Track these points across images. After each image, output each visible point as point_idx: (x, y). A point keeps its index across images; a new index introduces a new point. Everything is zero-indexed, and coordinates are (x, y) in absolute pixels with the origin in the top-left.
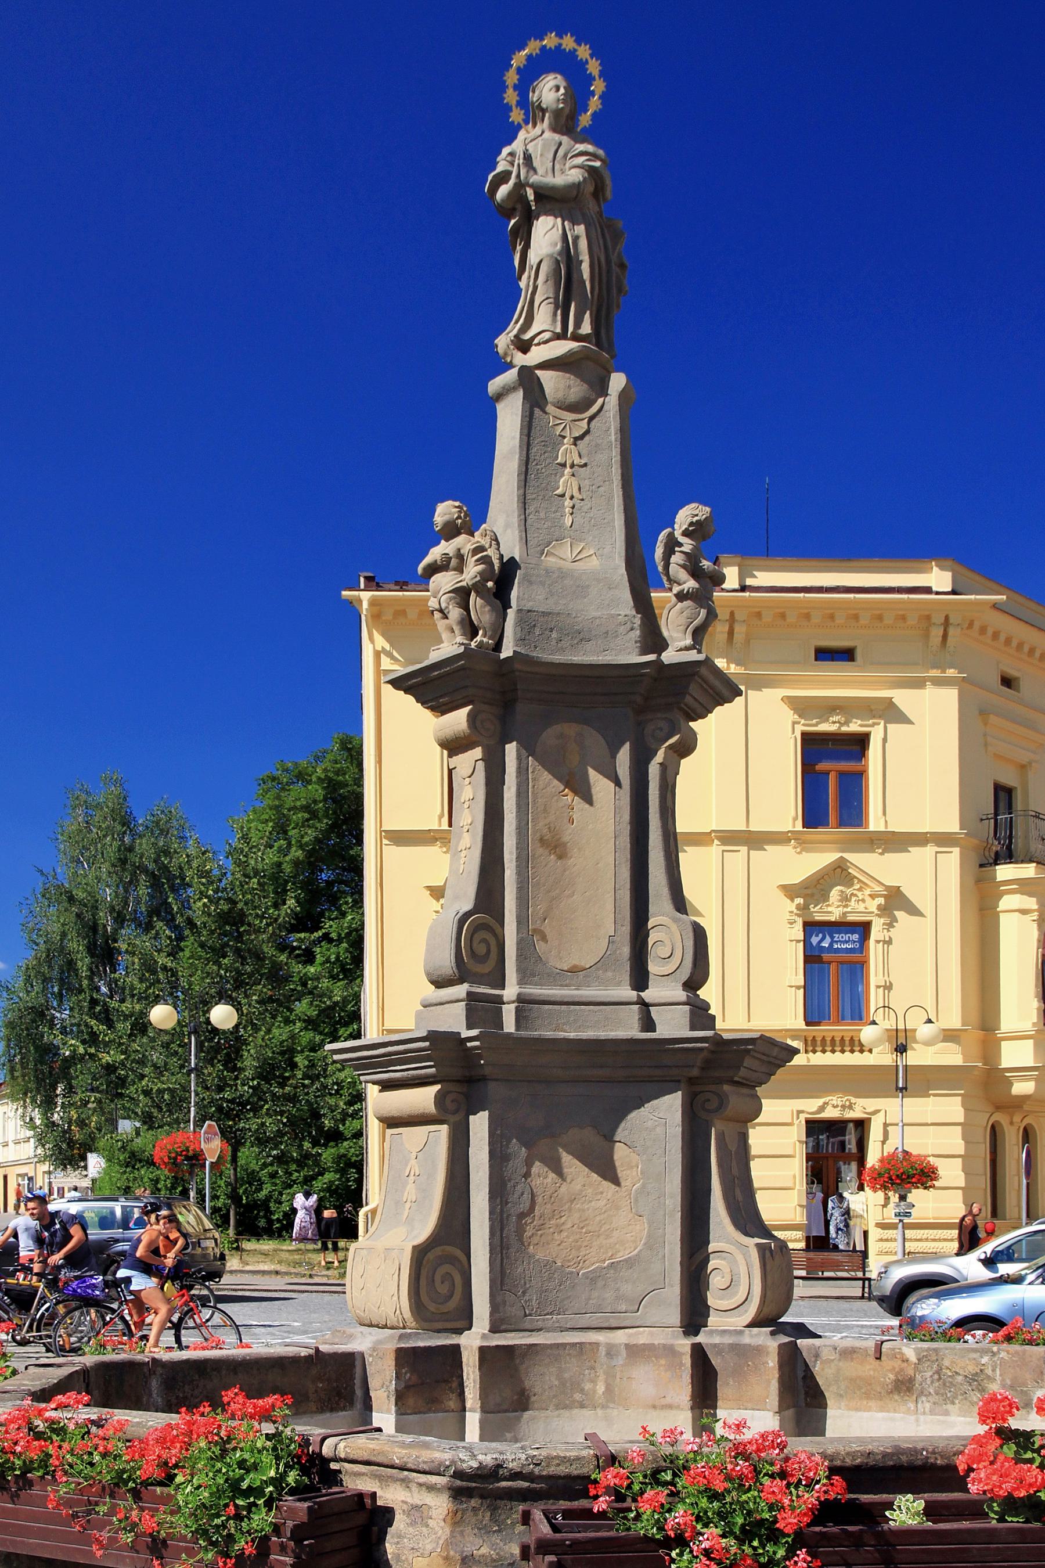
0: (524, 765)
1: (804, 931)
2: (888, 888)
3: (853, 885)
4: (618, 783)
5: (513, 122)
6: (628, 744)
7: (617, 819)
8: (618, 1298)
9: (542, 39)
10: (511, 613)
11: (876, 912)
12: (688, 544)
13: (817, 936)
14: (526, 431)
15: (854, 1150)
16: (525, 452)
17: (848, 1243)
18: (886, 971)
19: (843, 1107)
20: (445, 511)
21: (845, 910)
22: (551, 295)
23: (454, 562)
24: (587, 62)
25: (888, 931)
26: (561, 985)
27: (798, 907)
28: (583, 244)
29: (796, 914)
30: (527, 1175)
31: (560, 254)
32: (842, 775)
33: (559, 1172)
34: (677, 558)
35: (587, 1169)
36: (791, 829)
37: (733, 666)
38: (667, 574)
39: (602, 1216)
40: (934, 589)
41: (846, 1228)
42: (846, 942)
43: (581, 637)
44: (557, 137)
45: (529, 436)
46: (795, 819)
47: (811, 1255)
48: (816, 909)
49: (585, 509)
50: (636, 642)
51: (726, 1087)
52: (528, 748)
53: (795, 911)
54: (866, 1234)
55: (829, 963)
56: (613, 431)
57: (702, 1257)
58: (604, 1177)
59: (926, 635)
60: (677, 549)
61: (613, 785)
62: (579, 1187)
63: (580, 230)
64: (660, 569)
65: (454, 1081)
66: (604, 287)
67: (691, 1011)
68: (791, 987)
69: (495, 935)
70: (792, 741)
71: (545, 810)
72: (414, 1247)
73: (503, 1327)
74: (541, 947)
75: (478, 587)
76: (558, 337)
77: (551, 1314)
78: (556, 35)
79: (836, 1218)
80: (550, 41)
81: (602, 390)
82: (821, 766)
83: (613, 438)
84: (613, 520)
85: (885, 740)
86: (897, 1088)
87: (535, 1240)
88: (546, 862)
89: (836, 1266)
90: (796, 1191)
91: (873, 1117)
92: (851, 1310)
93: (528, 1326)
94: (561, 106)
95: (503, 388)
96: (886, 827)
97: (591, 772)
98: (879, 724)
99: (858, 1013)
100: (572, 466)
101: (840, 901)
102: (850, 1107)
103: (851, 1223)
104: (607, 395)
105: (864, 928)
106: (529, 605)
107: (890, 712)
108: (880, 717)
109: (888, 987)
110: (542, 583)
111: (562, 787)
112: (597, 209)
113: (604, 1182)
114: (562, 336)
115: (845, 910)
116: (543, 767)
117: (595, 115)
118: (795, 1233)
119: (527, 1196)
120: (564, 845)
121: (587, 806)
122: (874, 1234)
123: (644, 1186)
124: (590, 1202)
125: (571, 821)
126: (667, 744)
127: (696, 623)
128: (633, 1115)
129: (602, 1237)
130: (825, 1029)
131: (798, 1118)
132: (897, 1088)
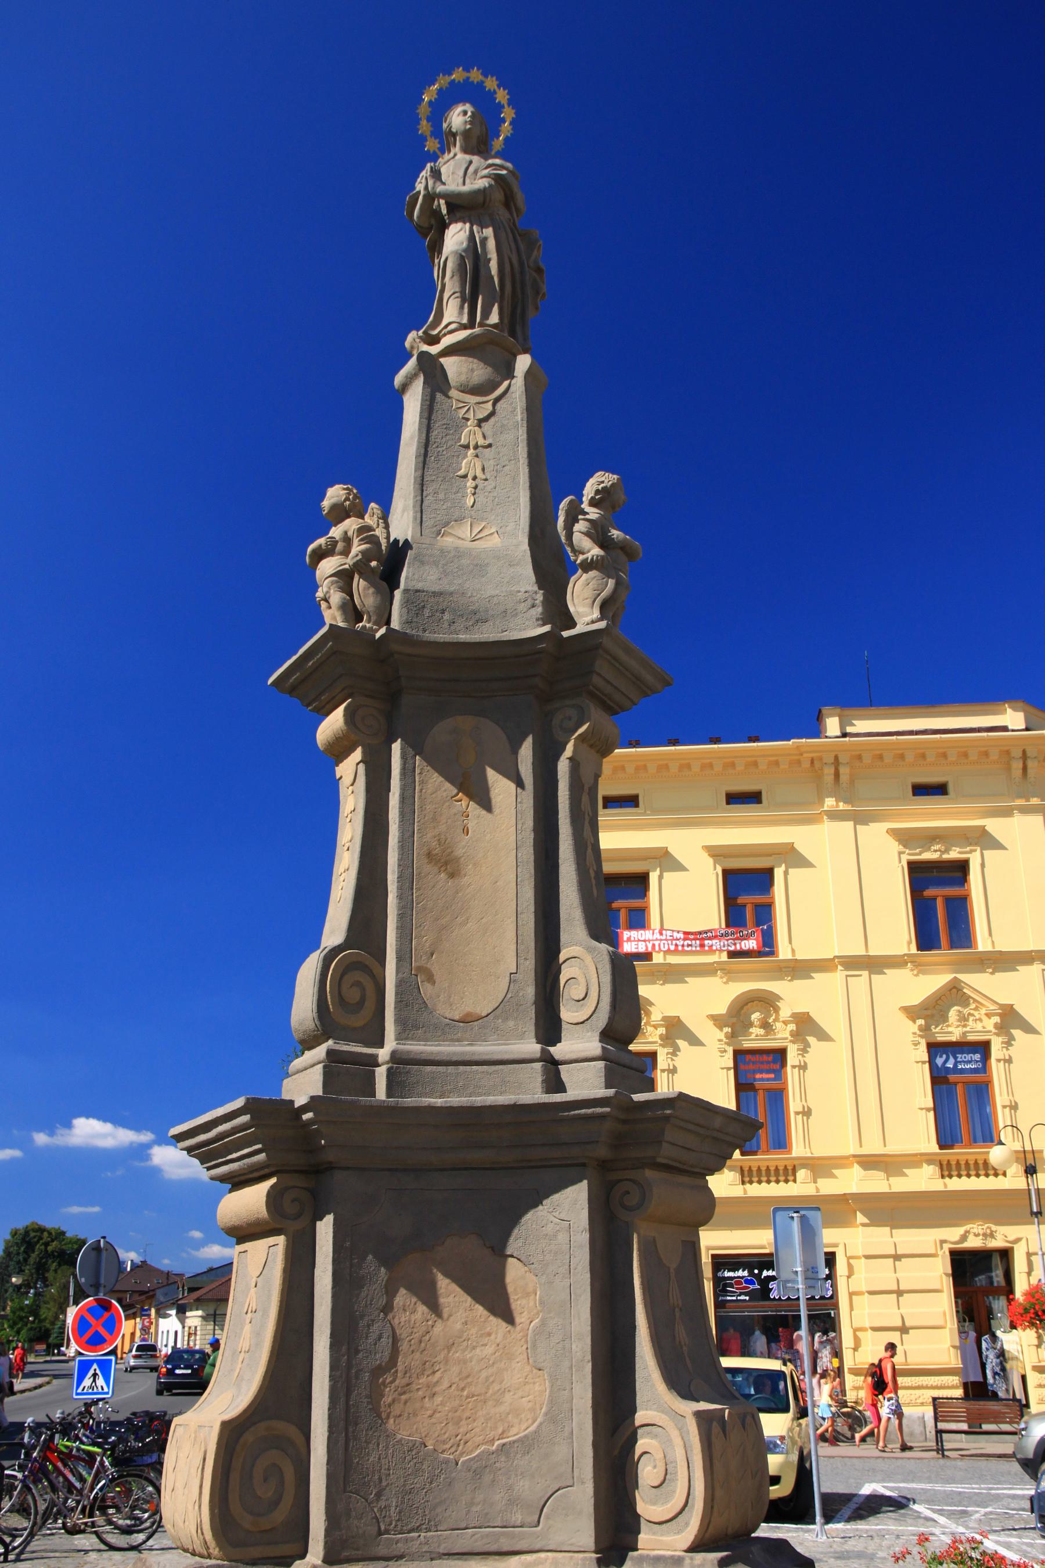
0: (409, 766)
1: (929, 1052)
2: (1002, 1006)
3: (968, 1005)
4: (520, 784)
5: (429, 151)
6: (531, 736)
7: (519, 826)
8: (512, 1502)
9: (451, 74)
10: (398, 593)
11: (994, 1030)
12: (593, 513)
13: (941, 1057)
14: (426, 415)
15: (1003, 1283)
16: (424, 435)
17: (1007, 1390)
18: (1010, 1090)
19: (985, 1235)
20: (335, 494)
21: (965, 1029)
22: (457, 290)
23: (340, 546)
24: (495, 92)
25: (1008, 1049)
26: (452, 1040)
27: (920, 1028)
28: (491, 244)
29: (920, 1036)
30: (387, 1308)
31: (465, 250)
32: (949, 901)
33: (435, 1307)
34: (580, 526)
35: (469, 1299)
36: (906, 952)
37: (841, 804)
38: (571, 545)
39: (490, 1370)
40: (1010, 728)
41: (1003, 1372)
42: (969, 1061)
43: (478, 618)
44: (468, 157)
45: (429, 419)
46: (910, 943)
47: (967, 1404)
48: (937, 1030)
49: (489, 488)
50: (537, 620)
51: (649, 1173)
52: (415, 746)
53: (918, 1032)
54: (1024, 1378)
55: (955, 1084)
56: (519, 410)
57: (628, 1433)
58: (493, 1310)
59: (1008, 769)
60: (580, 517)
61: (513, 786)
62: (458, 1326)
63: (489, 232)
64: (563, 539)
65: (296, 1172)
66: (518, 286)
67: (606, 1066)
68: (921, 1109)
69: (373, 976)
70: (900, 869)
71: (434, 819)
72: (225, 1424)
73: (345, 1554)
74: (426, 990)
75: (360, 568)
76: (464, 327)
77: (417, 1529)
78: (463, 70)
79: (992, 1361)
80: (458, 75)
81: (509, 372)
82: (929, 892)
83: (519, 418)
84: (518, 498)
85: (983, 865)
86: (1032, 1213)
87: (397, 1409)
88: (434, 883)
89: (997, 1418)
90: (947, 1330)
91: (1015, 1246)
92: (1009, 1473)
93: (382, 1551)
94: (468, 126)
95: (406, 377)
96: (993, 947)
97: (491, 773)
98: (975, 851)
99: (989, 1136)
100: (476, 447)
101: (959, 1021)
102: (992, 1235)
103: (1008, 1366)
104: (513, 377)
105: (983, 1048)
106: (419, 586)
107: (985, 840)
108: (976, 844)
109: (1014, 1107)
110: (436, 564)
111: (455, 791)
112: (507, 215)
113: (492, 1318)
114: (471, 324)
115: (965, 1029)
116: (433, 768)
117: (506, 139)
118: (951, 1378)
119: (386, 1341)
120: (457, 860)
121: (484, 812)
122: (1033, 1379)
123: (543, 1323)
124: (474, 1348)
125: (466, 831)
126: (576, 734)
127: (605, 594)
128: (530, 1218)
129: (490, 1403)
130: (958, 1153)
131: (942, 1248)
132: (1032, 1213)
